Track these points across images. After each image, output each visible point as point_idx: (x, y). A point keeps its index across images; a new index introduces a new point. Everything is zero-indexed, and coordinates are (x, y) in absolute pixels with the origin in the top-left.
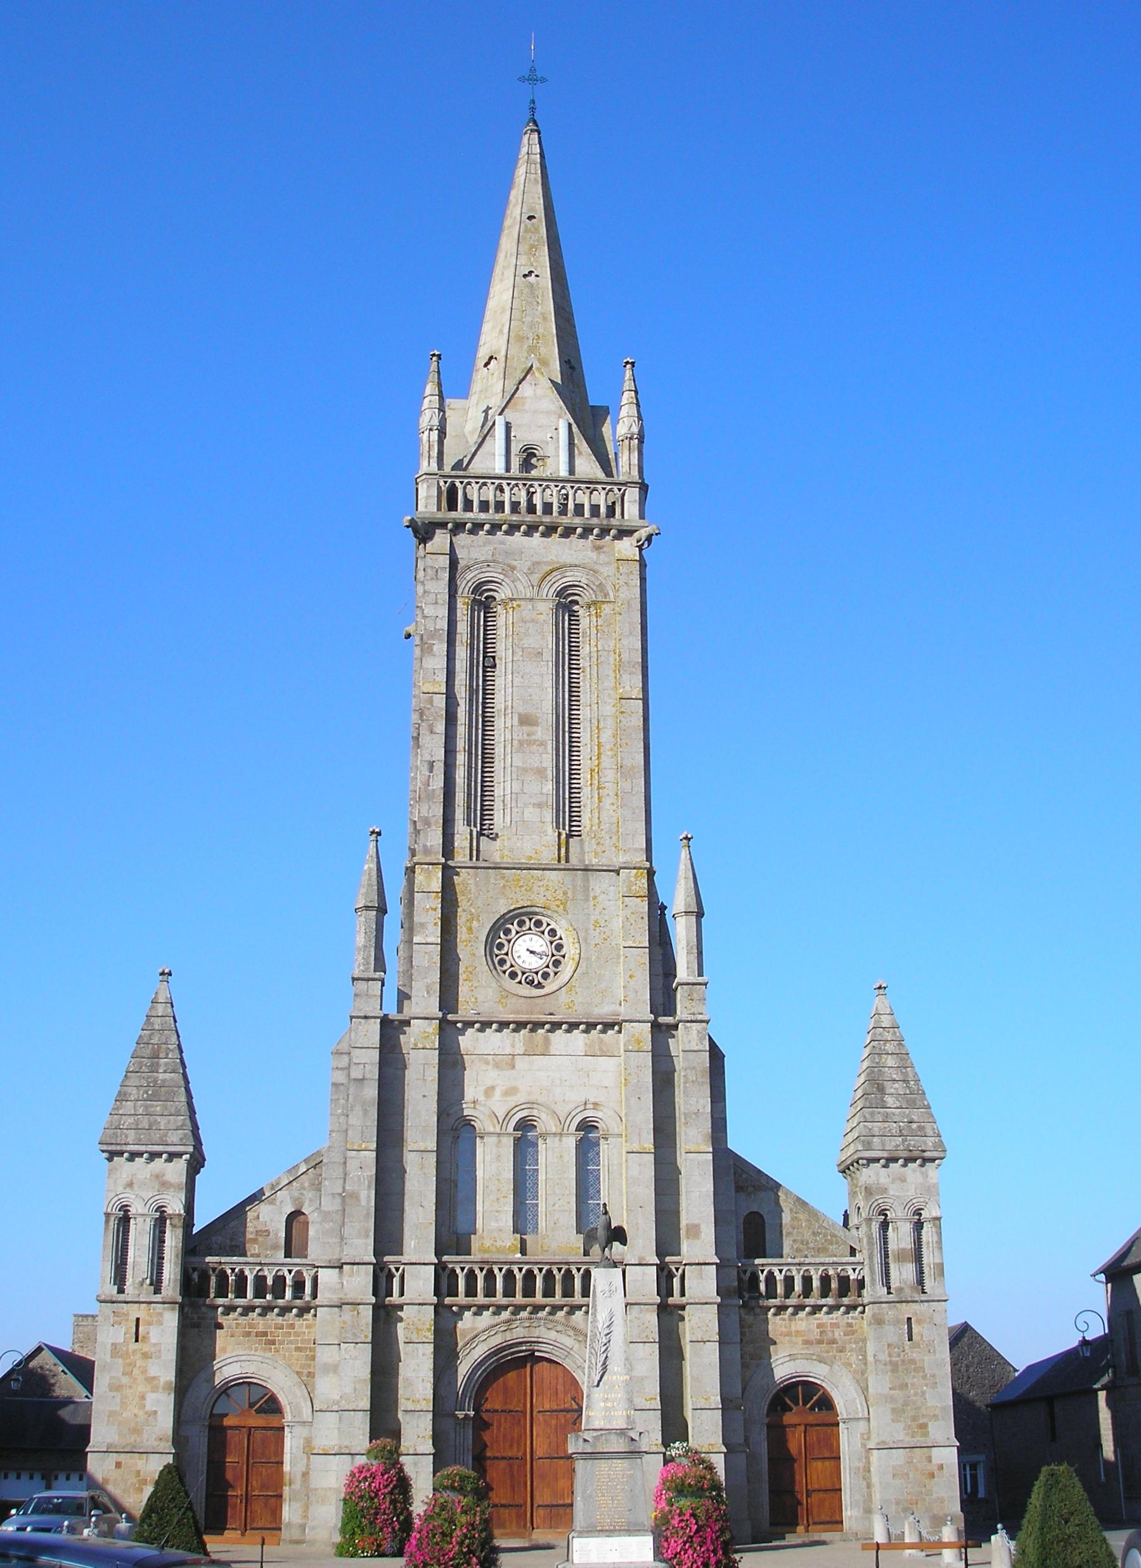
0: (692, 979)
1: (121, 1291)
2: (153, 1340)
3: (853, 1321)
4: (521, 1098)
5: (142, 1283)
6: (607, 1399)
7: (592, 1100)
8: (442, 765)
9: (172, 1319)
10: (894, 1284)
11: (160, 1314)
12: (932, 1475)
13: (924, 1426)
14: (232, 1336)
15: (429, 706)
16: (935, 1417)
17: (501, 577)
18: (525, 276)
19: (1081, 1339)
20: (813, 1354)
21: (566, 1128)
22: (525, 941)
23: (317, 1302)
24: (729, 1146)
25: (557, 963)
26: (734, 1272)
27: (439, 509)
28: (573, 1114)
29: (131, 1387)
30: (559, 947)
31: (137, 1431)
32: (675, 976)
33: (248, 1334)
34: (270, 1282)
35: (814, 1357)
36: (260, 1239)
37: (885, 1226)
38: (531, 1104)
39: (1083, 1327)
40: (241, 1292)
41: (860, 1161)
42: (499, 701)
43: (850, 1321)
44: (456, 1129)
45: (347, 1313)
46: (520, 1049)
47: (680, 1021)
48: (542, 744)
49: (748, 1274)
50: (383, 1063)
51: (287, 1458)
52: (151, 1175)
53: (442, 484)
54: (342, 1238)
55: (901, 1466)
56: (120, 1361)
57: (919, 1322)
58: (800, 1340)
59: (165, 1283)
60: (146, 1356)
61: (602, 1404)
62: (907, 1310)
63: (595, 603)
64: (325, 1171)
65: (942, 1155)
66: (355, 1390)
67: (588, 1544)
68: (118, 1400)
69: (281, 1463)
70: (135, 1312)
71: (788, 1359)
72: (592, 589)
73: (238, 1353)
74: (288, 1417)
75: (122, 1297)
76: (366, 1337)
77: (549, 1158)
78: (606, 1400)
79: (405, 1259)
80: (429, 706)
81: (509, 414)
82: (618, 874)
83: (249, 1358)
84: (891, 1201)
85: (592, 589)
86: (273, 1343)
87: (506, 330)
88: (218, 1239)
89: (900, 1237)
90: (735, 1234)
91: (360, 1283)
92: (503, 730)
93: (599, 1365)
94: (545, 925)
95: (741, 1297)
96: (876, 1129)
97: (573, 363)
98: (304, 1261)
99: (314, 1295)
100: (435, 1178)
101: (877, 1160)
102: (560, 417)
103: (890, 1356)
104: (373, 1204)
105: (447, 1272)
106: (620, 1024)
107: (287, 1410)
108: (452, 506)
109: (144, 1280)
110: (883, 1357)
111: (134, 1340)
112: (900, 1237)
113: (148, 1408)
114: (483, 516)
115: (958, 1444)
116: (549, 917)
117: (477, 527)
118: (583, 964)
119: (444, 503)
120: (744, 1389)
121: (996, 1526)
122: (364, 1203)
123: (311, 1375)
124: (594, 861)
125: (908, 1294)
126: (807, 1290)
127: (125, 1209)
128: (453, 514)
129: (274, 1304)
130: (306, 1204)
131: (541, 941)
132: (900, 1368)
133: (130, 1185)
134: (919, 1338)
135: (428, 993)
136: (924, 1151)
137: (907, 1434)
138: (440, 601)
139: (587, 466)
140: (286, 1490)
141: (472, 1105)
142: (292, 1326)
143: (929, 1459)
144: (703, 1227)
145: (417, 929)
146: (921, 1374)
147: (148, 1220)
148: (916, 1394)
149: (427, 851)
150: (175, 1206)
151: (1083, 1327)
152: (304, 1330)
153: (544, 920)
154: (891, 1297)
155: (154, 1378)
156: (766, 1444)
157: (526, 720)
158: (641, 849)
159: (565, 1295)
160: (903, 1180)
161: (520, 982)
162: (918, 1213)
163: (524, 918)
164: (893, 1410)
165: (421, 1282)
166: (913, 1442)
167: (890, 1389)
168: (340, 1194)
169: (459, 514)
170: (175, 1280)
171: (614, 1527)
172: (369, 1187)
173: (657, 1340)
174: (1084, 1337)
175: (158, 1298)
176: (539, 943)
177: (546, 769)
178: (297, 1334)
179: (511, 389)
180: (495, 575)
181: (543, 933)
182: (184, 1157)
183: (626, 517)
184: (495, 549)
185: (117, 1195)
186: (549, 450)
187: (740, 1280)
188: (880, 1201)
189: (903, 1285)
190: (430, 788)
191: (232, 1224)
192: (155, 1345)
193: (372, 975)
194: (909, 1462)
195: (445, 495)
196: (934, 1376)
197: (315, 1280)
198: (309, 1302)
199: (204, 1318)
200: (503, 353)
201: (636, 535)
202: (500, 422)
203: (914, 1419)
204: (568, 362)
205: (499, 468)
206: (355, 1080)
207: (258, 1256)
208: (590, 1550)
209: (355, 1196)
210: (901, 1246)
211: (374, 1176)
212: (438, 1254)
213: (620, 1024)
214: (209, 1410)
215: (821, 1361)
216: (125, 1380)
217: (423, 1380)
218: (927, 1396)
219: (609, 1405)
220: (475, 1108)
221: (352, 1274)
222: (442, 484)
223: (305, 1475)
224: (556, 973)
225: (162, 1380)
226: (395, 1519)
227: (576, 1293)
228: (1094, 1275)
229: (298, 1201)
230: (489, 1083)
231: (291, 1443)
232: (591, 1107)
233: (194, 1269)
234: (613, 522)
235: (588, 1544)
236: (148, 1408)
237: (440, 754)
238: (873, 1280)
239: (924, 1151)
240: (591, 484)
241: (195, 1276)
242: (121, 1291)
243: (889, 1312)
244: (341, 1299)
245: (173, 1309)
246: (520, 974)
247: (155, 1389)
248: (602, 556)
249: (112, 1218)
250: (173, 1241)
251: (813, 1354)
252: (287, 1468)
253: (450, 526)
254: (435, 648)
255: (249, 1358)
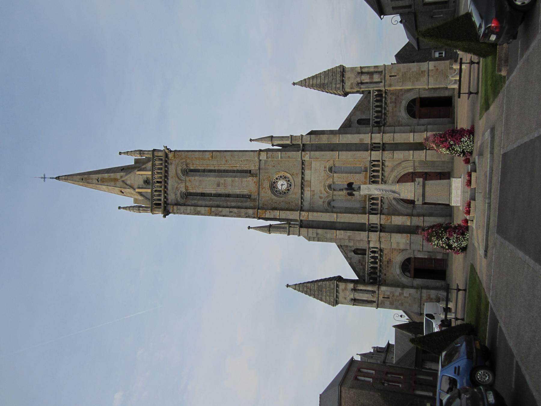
0: (290, 140)
1: (374, 302)
2: (389, 294)
3: (390, 93)
4: (322, 189)
5: (373, 296)
6: (404, 192)
7: (324, 169)
8: (230, 209)
9: (383, 288)
10: (379, 80)
11: (382, 291)
12: (437, 69)
13: (422, 72)
14: (388, 271)
15: (214, 212)
16: (420, 68)
17: (179, 191)
18: (98, 182)
19: (400, 23)
20: (399, 105)
21: (331, 176)
22: (279, 185)
23: (379, 247)
24: (338, 129)
25: (285, 178)
26: (374, 128)
27: (160, 208)
28: (327, 174)
29: (402, 300)
30: (281, 177)
31: (415, 299)
32: (289, 144)
33: (388, 267)
34: (373, 260)
35: (400, 105)
36: (361, 262)
37: (362, 83)
38: (325, 186)
39: (396, 22)
40: (376, 268)
41: (343, 91)
42: (213, 192)
43: (390, 94)
44: (331, 207)
45: (382, 240)
46: (309, 189)
47: (302, 143)
48: (225, 180)
49: (374, 124)
50: (312, 227)
51: (423, 257)
52: (343, 292)
53: (154, 207)
54: (361, 240)
55: (434, 79)
56: (395, 303)
57: (391, 73)
58: (395, 109)
59: (373, 289)
60: (393, 296)
61: (406, 193)
62: (387, 77)
63: (186, 165)
64: (342, 244)
65: (342, 66)
66: (404, 238)
67: (454, 200)
68: (406, 304)
69: (425, 258)
70: (381, 298)
71: (400, 113)
72: (182, 165)
73: (393, 270)
74: (412, 256)
75: (377, 302)
76: (389, 235)
77: (339, 181)
78: (405, 192)
79: (367, 223)
80: (214, 212)
81: (136, 186)
82: (261, 160)
83: (395, 266)
84: (355, 81)
85: (182, 165)
86: (390, 260)
87: (113, 187)
88: (361, 274)
89: (366, 78)
90: (363, 128)
91: (374, 236)
92: (221, 190)
93: (393, 194)
94: (275, 181)
95: (381, 126)
96: (334, 86)
97: (122, 168)
98: (367, 250)
99: (377, 248)
100: (345, 214)
101: (343, 86)
102: (136, 173)
103: (400, 82)
104: (351, 232)
105: (371, 211)
106: (302, 160)
107: (409, 256)
108: (160, 204)
109: (372, 295)
110: (401, 84)
111: (389, 299)
112: (366, 78)
113: (408, 295)
114: (162, 196)
115: (428, 61)
116: (273, 180)
117: (165, 197)
118: (286, 170)
119: (159, 207)
120: (409, 126)
121: (455, 52)
122: (351, 234)
123: (400, 250)
124: (257, 167)
125: (382, 76)
126: (380, 106)
127: (352, 300)
128: (162, 204)
129: (379, 259)
130: (351, 249)
131: (279, 182)
132: (404, 79)
133: (345, 298)
134: (395, 73)
135: (293, 214)
136: (341, 72)
137: (424, 77)
138: (186, 208)
139: (149, 165)
140: (433, 257)
141: (324, 203)
142: (386, 254)
143: (432, 70)
144: (361, 137)
145: (275, 217)
146: (406, 73)
147: (355, 294)
148: (412, 74)
149: (254, 214)
150: (351, 286)
151: (396, 22)
152: (387, 251)
153: (273, 181)
154: (383, 82)
155: (400, 294)
156: (425, 119)
157: (218, 185)
158: (254, 153)
159: (379, 178)
160: (349, 78)
161: (291, 188)
162: (359, 73)
163: (273, 187)
164: (417, 81)
165: (374, 219)
166: (426, 75)
167: (410, 82)
168: (349, 240)
169: (162, 202)
170: (372, 287)
171: (448, 191)
172: (346, 232)
173: (393, 151)
174: (399, 22)
175: (377, 292)
176: (280, 183)
177: (232, 180)
178: (388, 253)
179: (128, 187)
180: (179, 193)
181: (277, 181)
182: (338, 283)
183: (162, 155)
184: (172, 193)
185: (348, 302)
186: (145, 176)
187: (376, 127)
188: (355, 85)
189: (380, 78)
190: (237, 212)
191: (357, 270)
192: (390, 293)
193: (288, 230)
194: (433, 76)
195: (157, 206)
196: (407, 69)
197: (373, 248)
198: (379, 249)
199: (383, 279)
200: (119, 188)
201: (167, 153)
202: (137, 190)
203: (420, 75)
204: (122, 170)
205: (149, 191)
206: (317, 235)
207: (366, 263)
208: (456, 200)
209: (349, 237)
210: (368, 79)
211: (344, 231)
212: (366, 214)
213: (302, 160)
214: (409, 278)
215: (401, 102)
216: (400, 302)
217: (402, 219)
218: (413, 71)
219: (406, 191)
220: (325, 202)
221: (371, 238)
222: (154, 207)
223: (428, 252)
224: (288, 178)
225: (400, 291)
226: (443, 242)
227: (378, 174)
228: (381, 19)
229: (351, 251)
230: (318, 197)
231: (419, 256)
232: (325, 169)
233: (369, 281)
234: (164, 159)
235: (454, 200)
236: (408, 295)
237: (228, 209)
238: (378, 87)
239: (341, 72)
240: (153, 165)
241: (371, 281)
242: (374, 302)
243: (388, 82)
244: (378, 241)
245: (380, 288)
246: (288, 188)
247: (403, 294)
248: (173, 163)
249: (355, 303)
250: (361, 287)
251: (399, 105)
252: (426, 257)
253: (165, 205)
254: (199, 210)
255: (395, 266)
